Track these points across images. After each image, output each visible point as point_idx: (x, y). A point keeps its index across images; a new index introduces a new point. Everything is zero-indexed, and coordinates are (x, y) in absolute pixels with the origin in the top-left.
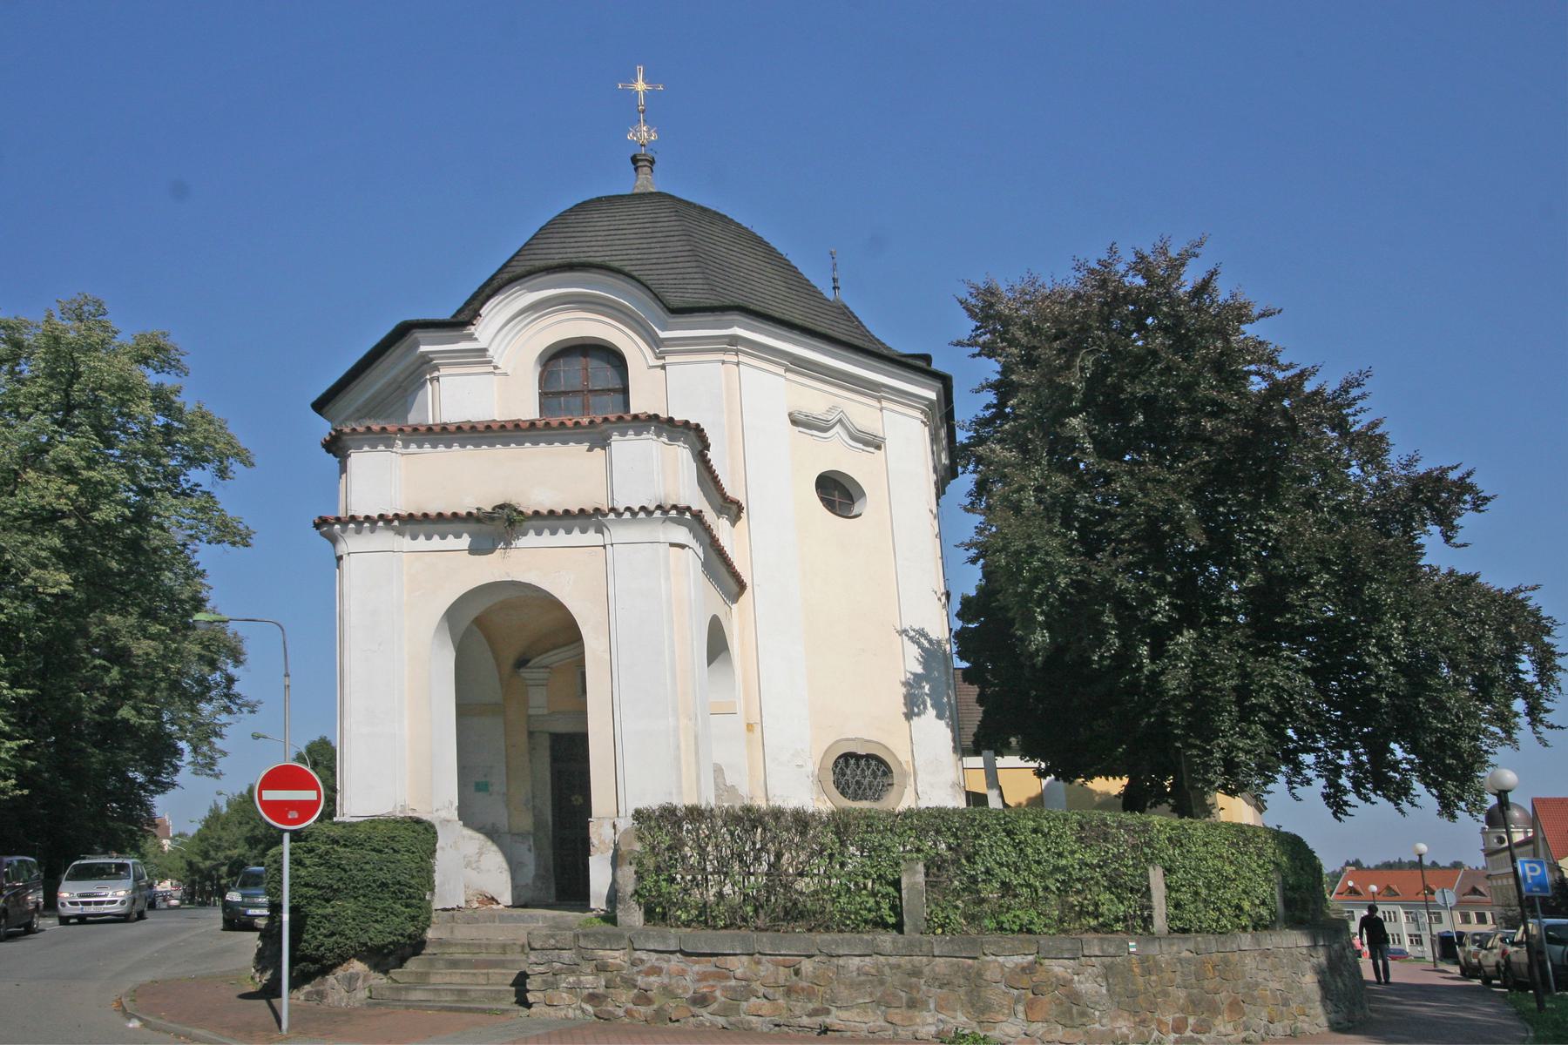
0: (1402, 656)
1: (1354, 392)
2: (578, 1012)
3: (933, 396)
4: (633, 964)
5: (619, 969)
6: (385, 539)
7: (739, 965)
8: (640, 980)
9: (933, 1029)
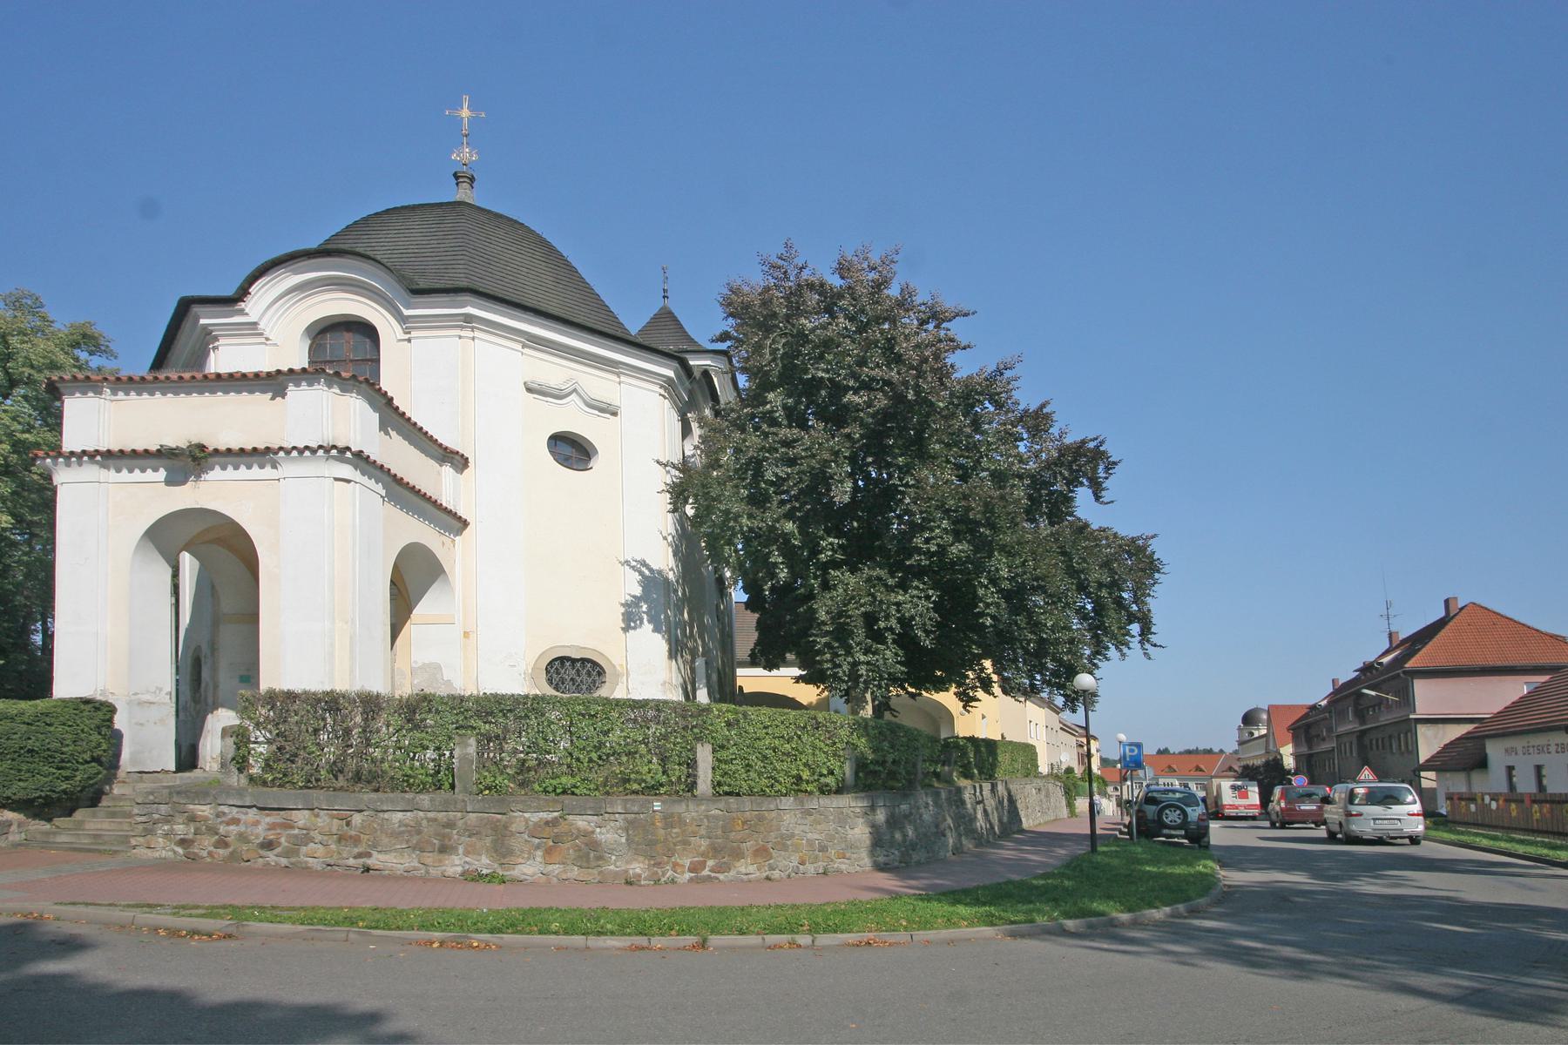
0: (1006, 585)
1: (1008, 374)
2: (170, 854)
3: (671, 374)
4: (218, 816)
5: (206, 819)
6: (91, 472)
7: (301, 818)
8: (222, 829)
9: (459, 869)
